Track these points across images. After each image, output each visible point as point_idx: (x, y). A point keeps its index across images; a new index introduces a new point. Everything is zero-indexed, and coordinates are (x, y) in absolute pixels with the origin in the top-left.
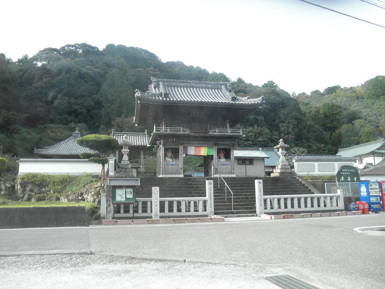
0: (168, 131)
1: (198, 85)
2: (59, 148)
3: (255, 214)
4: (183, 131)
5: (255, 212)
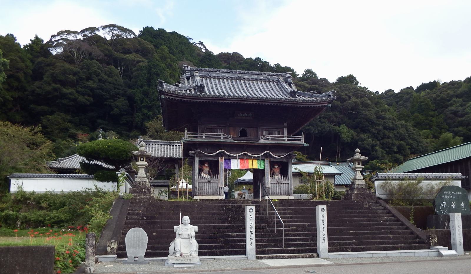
0: (204, 137)
1: (246, 77)
2: (77, 159)
3: (315, 254)
4: (224, 138)
5: (315, 251)
